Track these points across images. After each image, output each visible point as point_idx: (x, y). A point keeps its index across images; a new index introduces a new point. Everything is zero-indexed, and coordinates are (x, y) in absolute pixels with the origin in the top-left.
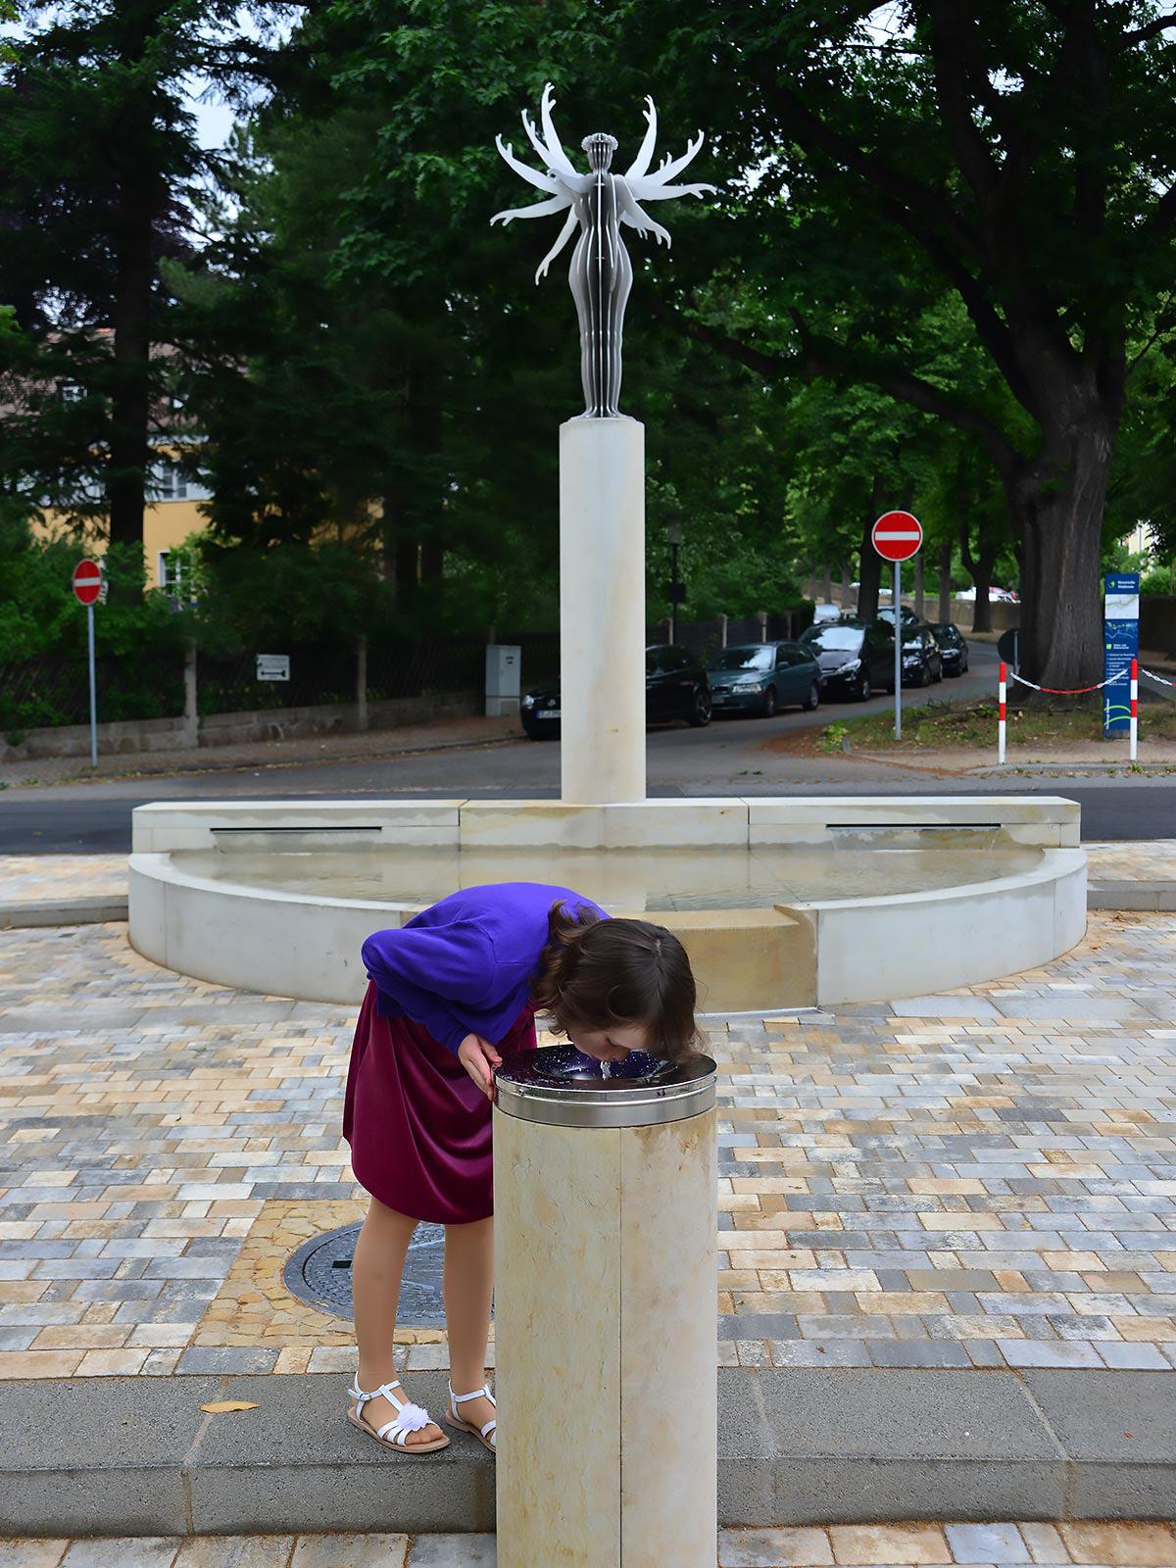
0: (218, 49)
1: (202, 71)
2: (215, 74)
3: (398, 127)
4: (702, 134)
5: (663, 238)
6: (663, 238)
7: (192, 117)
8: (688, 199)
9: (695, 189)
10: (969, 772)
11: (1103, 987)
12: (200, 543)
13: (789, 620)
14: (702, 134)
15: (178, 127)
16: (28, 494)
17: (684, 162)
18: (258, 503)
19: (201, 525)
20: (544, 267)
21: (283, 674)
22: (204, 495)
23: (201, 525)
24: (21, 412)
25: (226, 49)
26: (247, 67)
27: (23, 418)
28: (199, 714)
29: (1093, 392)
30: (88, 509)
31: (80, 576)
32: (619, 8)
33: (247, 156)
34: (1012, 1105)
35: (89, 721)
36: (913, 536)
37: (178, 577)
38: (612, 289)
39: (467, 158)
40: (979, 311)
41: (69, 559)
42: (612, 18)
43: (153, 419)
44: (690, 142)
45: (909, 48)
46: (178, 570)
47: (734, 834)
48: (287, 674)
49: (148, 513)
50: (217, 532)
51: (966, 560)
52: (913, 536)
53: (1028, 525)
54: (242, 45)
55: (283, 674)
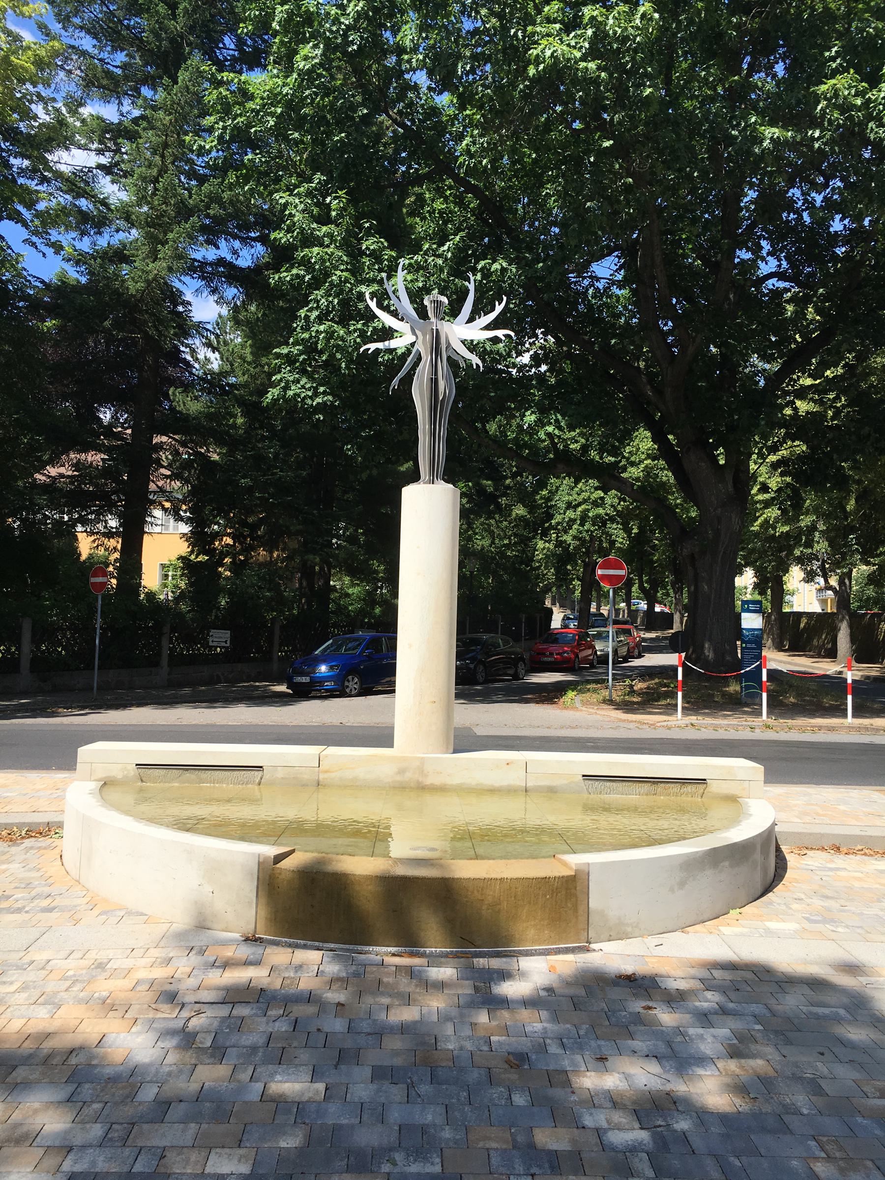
0: (206, 264)
1: (195, 275)
2: (203, 278)
3: (311, 310)
4: (505, 298)
5: (477, 365)
6: (477, 365)
7: (189, 303)
8: (495, 340)
9: (500, 333)
10: (658, 725)
11: (807, 925)
12: (181, 558)
13: (538, 619)
14: (505, 298)
15: (181, 309)
16: (692, 588)
17: (492, 316)
18: (217, 535)
19: (183, 548)
20: (395, 382)
21: (226, 642)
22: (185, 528)
23: (183, 548)
24: (70, 473)
25: (211, 264)
26: (222, 275)
27: (68, 477)
28: (169, 666)
29: (731, 489)
30: (109, 535)
31: (94, 576)
32: (450, 241)
33: (226, 333)
34: (182, 278)
35: (93, 668)
36: (622, 572)
37: (170, 578)
38: (441, 398)
39: (352, 328)
40: (658, 437)
41: (96, 566)
42: (446, 248)
43: (153, 481)
44: (497, 303)
45: (621, 285)
46: (170, 573)
47: (515, 778)
48: (228, 642)
49: (146, 538)
50: (192, 552)
51: (641, 587)
52: (622, 572)
53: (690, 568)
54: (221, 261)
55: (226, 642)
